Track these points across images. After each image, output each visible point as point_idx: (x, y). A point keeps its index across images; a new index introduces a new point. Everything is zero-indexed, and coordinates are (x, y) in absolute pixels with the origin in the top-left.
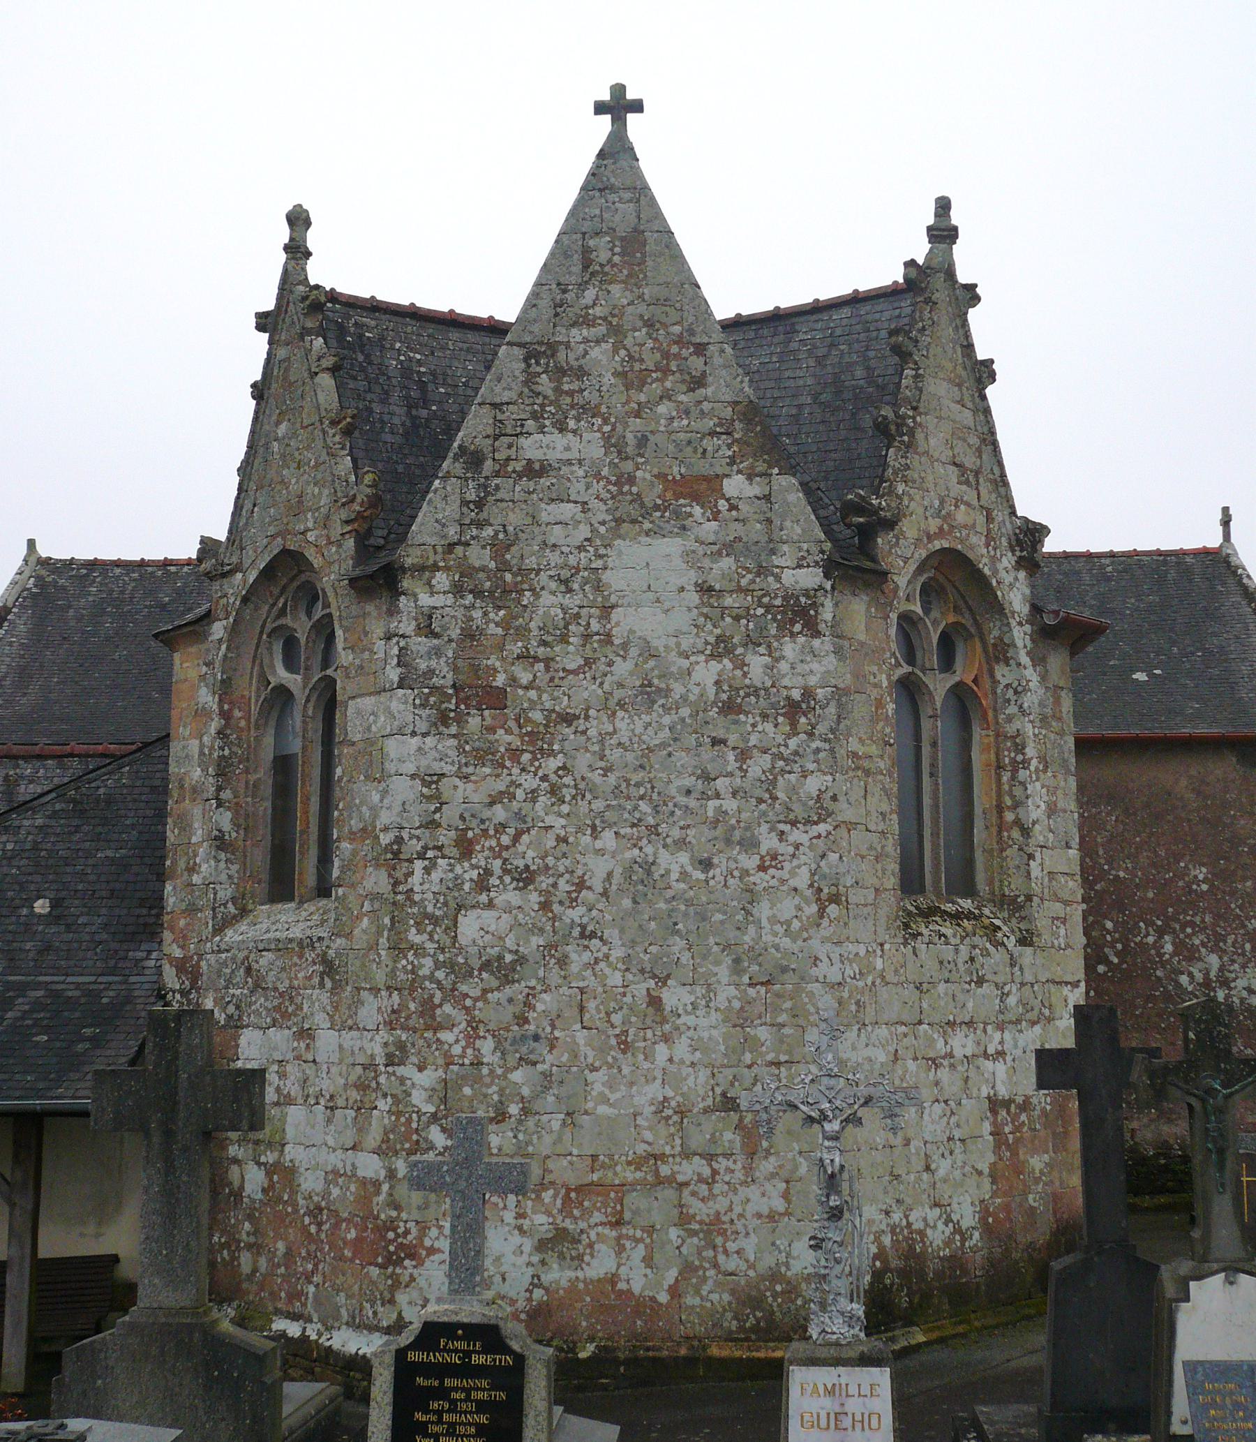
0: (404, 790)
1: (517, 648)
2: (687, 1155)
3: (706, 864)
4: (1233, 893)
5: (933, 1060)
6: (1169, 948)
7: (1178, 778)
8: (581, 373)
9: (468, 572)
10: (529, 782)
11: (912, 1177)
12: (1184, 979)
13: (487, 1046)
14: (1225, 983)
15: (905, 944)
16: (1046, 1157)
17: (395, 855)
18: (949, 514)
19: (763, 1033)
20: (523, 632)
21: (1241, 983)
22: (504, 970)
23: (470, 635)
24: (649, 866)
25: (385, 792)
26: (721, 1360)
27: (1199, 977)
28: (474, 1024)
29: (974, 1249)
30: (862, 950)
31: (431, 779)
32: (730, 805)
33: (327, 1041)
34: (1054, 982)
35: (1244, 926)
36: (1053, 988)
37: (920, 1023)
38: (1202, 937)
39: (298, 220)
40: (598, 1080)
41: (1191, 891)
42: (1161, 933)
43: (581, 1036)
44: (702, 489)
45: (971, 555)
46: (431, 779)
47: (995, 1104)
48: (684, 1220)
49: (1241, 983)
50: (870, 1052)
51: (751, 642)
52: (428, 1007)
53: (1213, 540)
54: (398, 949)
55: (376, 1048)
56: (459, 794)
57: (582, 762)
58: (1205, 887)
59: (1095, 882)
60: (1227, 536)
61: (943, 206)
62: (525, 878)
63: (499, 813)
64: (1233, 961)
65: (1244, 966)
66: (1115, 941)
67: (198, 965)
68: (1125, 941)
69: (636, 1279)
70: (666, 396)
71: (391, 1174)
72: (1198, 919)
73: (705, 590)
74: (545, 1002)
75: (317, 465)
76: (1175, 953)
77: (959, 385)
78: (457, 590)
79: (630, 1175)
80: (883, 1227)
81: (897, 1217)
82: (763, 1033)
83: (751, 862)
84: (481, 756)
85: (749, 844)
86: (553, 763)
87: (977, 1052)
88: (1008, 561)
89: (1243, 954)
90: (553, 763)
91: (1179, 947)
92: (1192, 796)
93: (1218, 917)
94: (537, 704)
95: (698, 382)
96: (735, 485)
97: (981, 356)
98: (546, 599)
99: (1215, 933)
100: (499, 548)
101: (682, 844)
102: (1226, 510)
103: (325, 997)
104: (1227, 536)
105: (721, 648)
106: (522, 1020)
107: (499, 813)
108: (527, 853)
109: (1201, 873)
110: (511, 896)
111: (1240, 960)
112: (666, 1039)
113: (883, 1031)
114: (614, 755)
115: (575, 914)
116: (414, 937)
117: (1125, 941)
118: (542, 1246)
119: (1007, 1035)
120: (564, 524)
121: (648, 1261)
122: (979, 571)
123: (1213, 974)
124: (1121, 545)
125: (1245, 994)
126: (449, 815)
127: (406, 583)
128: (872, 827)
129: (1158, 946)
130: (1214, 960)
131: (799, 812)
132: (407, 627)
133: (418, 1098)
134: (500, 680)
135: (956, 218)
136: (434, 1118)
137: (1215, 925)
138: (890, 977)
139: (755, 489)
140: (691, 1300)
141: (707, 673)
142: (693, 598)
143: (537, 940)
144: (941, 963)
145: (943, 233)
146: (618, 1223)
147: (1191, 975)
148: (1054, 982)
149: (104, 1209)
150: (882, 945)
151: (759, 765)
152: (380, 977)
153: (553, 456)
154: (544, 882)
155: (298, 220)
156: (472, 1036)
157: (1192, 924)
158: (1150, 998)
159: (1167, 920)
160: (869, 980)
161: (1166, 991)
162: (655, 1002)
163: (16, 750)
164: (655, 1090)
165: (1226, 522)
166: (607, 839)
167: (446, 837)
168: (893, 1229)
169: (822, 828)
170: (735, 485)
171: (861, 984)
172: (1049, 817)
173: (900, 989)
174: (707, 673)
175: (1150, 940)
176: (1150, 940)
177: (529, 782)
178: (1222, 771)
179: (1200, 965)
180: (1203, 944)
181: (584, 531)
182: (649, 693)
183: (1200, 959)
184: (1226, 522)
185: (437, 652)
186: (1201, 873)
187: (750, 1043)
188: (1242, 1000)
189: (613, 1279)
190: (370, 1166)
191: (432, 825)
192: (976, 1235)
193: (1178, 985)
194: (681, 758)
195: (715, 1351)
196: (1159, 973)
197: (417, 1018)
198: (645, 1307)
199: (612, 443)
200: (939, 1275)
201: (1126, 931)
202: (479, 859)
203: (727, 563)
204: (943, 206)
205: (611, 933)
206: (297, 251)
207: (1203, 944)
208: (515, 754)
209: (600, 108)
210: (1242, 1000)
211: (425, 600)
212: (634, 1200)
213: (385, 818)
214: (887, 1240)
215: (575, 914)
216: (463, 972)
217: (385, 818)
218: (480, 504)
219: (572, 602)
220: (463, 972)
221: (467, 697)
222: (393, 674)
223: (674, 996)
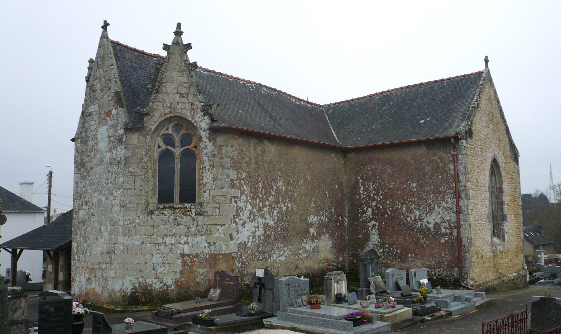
4: (424, 191)
5: (158, 244)
6: (405, 209)
7: (408, 155)
11: (148, 271)
12: (409, 219)
14: (421, 220)
15: (148, 216)
16: (206, 270)
18: (174, 107)
21: (425, 220)
26: (105, 308)
27: (413, 218)
29: (173, 290)
30: (131, 218)
32: (110, 185)
34: (212, 224)
35: (427, 202)
36: (211, 226)
37: (153, 235)
38: (414, 205)
41: (411, 191)
42: (402, 205)
45: (183, 116)
47: (183, 255)
49: (425, 220)
50: (133, 241)
53: (481, 67)
58: (415, 190)
59: (385, 189)
60: (487, 66)
61: (179, 25)
64: (423, 213)
65: (426, 215)
66: (390, 207)
68: (392, 207)
72: (413, 200)
73: (109, 137)
76: (406, 211)
77: (182, 72)
80: (136, 282)
81: (141, 280)
87: (176, 242)
88: (200, 114)
89: (426, 211)
91: (407, 209)
92: (412, 161)
93: (419, 199)
96: (114, 112)
97: (191, 61)
99: (418, 204)
102: (486, 57)
104: (487, 66)
105: (110, 151)
109: (414, 185)
111: (425, 212)
113: (138, 237)
117: (392, 207)
119: (189, 238)
122: (187, 120)
123: (417, 217)
125: (426, 223)
128: (137, 189)
129: (401, 209)
130: (417, 213)
131: (119, 187)
135: (182, 29)
137: (418, 201)
138: (141, 224)
140: (103, 295)
141: (108, 155)
144: (162, 220)
145: (178, 33)
147: (411, 218)
148: (212, 224)
150: (139, 217)
157: (412, 201)
158: (399, 225)
159: (404, 200)
160: (133, 225)
161: (403, 223)
165: (486, 61)
168: (139, 283)
169: (122, 190)
171: (130, 226)
172: (214, 181)
173: (145, 227)
174: (108, 155)
175: (399, 207)
176: (399, 207)
178: (422, 151)
179: (413, 214)
180: (415, 208)
183: (413, 213)
184: (486, 61)
186: (414, 185)
188: (426, 226)
192: (173, 287)
193: (407, 221)
195: (104, 306)
196: (402, 217)
200: (156, 295)
201: (393, 204)
204: (179, 25)
207: (415, 208)
210: (426, 226)
214: (137, 285)
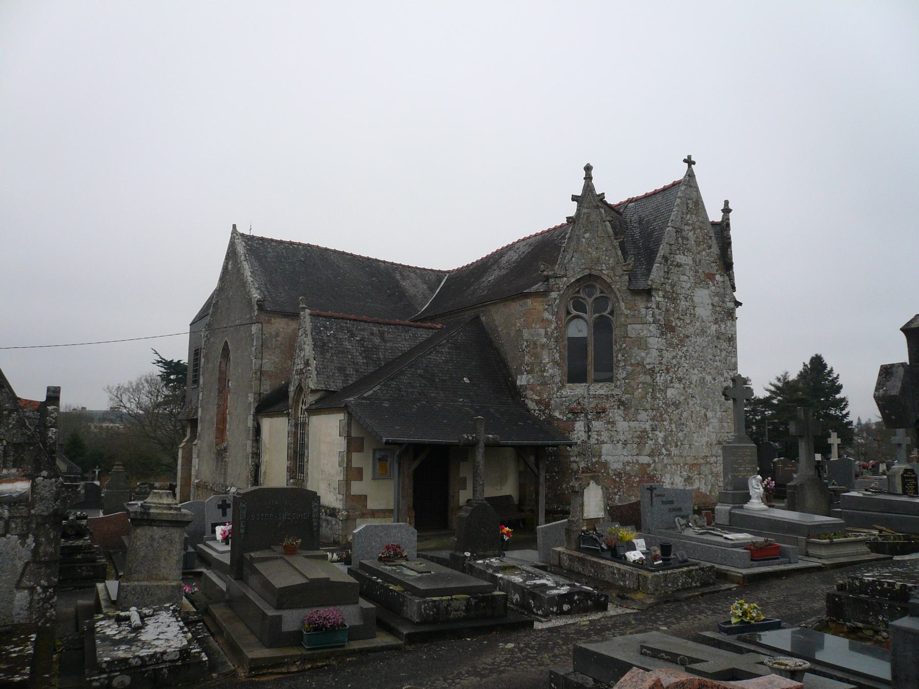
0: (655, 353)
1: (677, 315)
2: (712, 456)
3: (714, 379)
8: (687, 239)
9: (666, 292)
10: (680, 353)
13: (673, 426)
17: (652, 372)
19: (725, 424)
20: (678, 311)
22: (676, 405)
23: (667, 310)
24: (704, 379)
25: (647, 354)
28: (671, 420)
31: (660, 350)
32: (719, 364)
33: (622, 425)
39: (588, 169)
40: (695, 435)
43: (692, 424)
44: (711, 277)
46: (660, 350)
48: (712, 473)
51: (722, 321)
52: (661, 415)
54: (654, 398)
55: (648, 426)
56: (667, 355)
57: (691, 349)
61: (727, 203)
62: (680, 380)
63: (674, 362)
67: (549, 402)
69: (704, 489)
70: (704, 250)
71: (654, 461)
73: (713, 305)
74: (685, 414)
75: (606, 250)
78: (664, 297)
79: (702, 461)
82: (725, 424)
83: (722, 379)
84: (671, 345)
85: (722, 375)
86: (685, 349)
90: (685, 349)
94: (682, 332)
95: (710, 247)
96: (718, 277)
98: (683, 303)
100: (673, 286)
101: (710, 373)
103: (621, 412)
105: (716, 322)
106: (680, 419)
107: (674, 362)
108: (680, 374)
110: (677, 385)
112: (708, 425)
114: (697, 348)
115: (690, 391)
116: (658, 395)
118: (685, 480)
120: (685, 281)
121: (705, 484)
124: (365, 254)
126: (664, 361)
127: (653, 293)
132: (654, 306)
133: (660, 440)
134: (674, 324)
135: (730, 206)
136: (663, 446)
139: (721, 279)
141: (714, 327)
142: (711, 307)
143: (683, 397)
146: (700, 474)
149: (502, 481)
151: (724, 353)
152: (648, 406)
153: (683, 262)
154: (684, 381)
155: (588, 169)
156: (670, 424)
162: (706, 415)
163: (380, 320)
164: (706, 439)
166: (696, 371)
167: (664, 367)
170: (718, 277)
177: (680, 353)
181: (689, 285)
182: (703, 332)
185: (660, 314)
187: (723, 427)
189: (699, 489)
190: (644, 459)
191: (661, 363)
194: (709, 350)
197: (657, 419)
198: (705, 496)
199: (694, 261)
202: (671, 374)
203: (717, 298)
204: (727, 203)
205: (697, 396)
206: (588, 178)
208: (677, 345)
209: (685, 161)
211: (658, 299)
212: (703, 468)
213: (648, 360)
215: (690, 391)
216: (668, 405)
217: (648, 360)
218: (668, 273)
219: (687, 304)
220: (668, 405)
221: (667, 328)
222: (651, 320)
223: (710, 414)
